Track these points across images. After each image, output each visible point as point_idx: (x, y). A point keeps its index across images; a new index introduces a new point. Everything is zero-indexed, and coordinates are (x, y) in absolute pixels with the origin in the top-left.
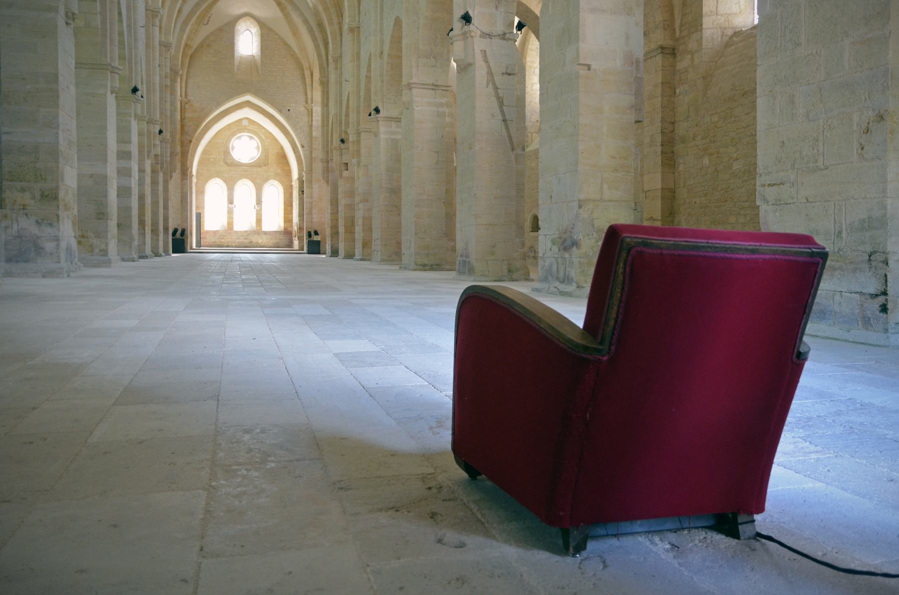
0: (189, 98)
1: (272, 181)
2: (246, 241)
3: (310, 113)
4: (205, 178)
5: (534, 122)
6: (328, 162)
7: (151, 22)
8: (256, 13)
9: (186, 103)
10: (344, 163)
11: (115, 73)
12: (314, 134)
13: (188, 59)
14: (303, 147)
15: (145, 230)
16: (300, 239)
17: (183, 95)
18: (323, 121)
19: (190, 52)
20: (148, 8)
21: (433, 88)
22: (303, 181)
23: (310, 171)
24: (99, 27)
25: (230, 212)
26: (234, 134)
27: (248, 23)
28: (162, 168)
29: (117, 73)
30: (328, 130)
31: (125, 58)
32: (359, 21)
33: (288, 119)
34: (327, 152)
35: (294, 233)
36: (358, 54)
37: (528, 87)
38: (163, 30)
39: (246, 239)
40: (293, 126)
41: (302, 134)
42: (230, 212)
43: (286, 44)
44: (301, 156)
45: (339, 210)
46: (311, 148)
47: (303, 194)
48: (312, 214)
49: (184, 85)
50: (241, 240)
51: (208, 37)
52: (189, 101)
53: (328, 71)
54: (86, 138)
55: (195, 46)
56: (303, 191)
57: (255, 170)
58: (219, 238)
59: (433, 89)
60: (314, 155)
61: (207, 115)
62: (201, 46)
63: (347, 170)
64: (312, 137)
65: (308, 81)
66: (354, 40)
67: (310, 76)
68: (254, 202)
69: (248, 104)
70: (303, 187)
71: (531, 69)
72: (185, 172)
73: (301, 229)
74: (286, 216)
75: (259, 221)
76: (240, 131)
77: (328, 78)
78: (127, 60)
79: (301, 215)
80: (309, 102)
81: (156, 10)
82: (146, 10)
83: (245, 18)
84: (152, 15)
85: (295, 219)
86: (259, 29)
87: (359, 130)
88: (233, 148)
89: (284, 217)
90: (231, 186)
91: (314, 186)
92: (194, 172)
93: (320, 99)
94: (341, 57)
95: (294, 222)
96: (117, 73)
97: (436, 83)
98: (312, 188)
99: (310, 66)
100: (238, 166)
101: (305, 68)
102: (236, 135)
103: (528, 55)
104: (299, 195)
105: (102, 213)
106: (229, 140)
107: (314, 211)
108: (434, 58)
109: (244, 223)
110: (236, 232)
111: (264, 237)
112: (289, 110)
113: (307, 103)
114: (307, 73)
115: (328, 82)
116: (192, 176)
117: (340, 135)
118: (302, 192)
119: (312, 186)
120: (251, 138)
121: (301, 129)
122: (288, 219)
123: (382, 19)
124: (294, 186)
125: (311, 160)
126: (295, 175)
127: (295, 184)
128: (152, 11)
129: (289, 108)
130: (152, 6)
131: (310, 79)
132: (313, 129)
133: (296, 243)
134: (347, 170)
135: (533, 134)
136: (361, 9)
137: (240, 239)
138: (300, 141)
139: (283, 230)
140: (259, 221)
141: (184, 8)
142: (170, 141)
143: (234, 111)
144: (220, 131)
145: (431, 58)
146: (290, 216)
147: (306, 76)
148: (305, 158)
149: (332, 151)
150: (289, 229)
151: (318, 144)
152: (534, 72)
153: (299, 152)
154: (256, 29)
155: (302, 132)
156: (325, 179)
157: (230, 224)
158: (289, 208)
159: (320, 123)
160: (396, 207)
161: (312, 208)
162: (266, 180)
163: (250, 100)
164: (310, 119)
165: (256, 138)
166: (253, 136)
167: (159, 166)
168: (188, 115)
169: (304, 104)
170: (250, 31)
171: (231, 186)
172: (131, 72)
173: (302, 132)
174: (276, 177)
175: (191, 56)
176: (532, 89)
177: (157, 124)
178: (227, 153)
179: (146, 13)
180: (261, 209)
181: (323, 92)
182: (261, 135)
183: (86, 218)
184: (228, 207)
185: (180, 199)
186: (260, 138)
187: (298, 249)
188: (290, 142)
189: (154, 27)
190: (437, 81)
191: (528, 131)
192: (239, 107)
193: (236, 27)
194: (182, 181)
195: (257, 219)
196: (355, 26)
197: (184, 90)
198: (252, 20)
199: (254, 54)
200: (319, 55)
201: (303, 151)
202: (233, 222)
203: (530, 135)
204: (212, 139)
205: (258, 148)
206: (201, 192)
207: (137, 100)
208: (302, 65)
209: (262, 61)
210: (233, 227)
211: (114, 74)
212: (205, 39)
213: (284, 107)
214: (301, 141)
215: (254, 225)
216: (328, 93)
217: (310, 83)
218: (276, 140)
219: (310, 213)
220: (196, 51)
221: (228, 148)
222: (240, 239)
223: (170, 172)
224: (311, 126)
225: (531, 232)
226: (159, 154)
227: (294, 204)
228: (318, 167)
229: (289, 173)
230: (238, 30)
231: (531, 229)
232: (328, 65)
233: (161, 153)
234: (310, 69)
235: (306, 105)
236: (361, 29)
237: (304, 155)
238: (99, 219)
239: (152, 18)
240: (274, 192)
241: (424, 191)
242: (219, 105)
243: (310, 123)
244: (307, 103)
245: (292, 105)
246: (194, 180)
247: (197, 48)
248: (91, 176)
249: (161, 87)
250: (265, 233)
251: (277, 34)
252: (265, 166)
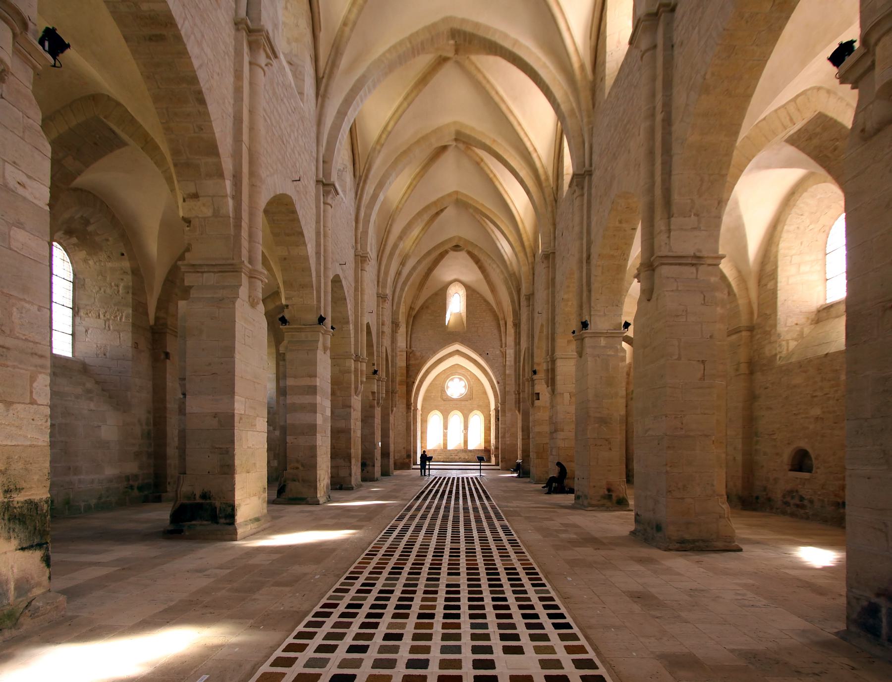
0: (413, 349)
1: (476, 412)
2: (457, 457)
3: (504, 355)
4: (426, 411)
5: (792, 326)
6: (520, 393)
7: (360, 267)
8: (464, 278)
9: (410, 353)
10: (536, 393)
11: (255, 278)
12: (507, 372)
13: (412, 319)
14: (498, 383)
15: (351, 463)
16: (497, 457)
17: (409, 347)
18: (515, 358)
19: (414, 313)
20: (357, 254)
21: (694, 262)
22: (499, 411)
23: (503, 403)
24: (231, 216)
25: (445, 435)
26: (448, 377)
27: (457, 287)
28: (378, 403)
29: (259, 279)
30: (519, 366)
31: (312, 287)
32: (555, 246)
33: (487, 361)
34: (519, 385)
35: (491, 451)
36: (553, 279)
37: (781, 282)
38: (380, 284)
39: (456, 456)
40: (491, 367)
41: (498, 372)
42: (445, 435)
43: (486, 301)
44: (497, 391)
45: (531, 437)
46: (505, 384)
47: (499, 421)
48: (505, 438)
49: (409, 339)
50: (453, 457)
51: (427, 301)
52: (413, 351)
53: (520, 314)
54: (210, 364)
55: (417, 309)
56: (498, 419)
57: (463, 403)
58: (438, 456)
59: (693, 265)
60: (507, 389)
61: (425, 362)
62: (422, 308)
63: (539, 399)
64: (505, 375)
65: (503, 329)
66: (549, 267)
67: (504, 325)
68: (462, 428)
69: (457, 352)
70: (499, 416)
71: (787, 258)
72: (409, 406)
73: (497, 448)
74: (486, 438)
75: (466, 442)
76: (452, 374)
77: (520, 319)
78: (314, 288)
79: (497, 437)
80: (503, 346)
81: (364, 255)
82: (355, 255)
83: (454, 283)
84: (361, 261)
85: (493, 441)
86: (465, 291)
87: (553, 357)
88: (448, 387)
89: (485, 439)
90: (446, 415)
91: (507, 415)
92: (419, 406)
93: (513, 344)
94: (533, 294)
95: (491, 443)
96: (259, 279)
97: (698, 254)
98: (505, 416)
99: (504, 316)
100: (451, 401)
101: (500, 319)
102: (449, 377)
103: (782, 239)
104: (496, 422)
105: (228, 466)
106: (445, 381)
107: (507, 435)
108: (697, 215)
109: (455, 443)
110: (449, 450)
111: (470, 454)
112: (488, 354)
113: (501, 347)
114: (502, 323)
115: (520, 324)
116: (416, 409)
117: (532, 366)
118: (497, 419)
119: (505, 415)
120: (461, 379)
121: (497, 369)
122: (487, 441)
123: (589, 217)
124: (492, 415)
125: (504, 393)
126: (493, 407)
127: (493, 413)
128: (361, 257)
129: (488, 352)
130: (360, 252)
131: (504, 327)
132: (507, 368)
133: (493, 459)
134: (539, 399)
135: (790, 341)
136: (556, 232)
137: (452, 455)
138: (496, 378)
139: (483, 449)
140: (466, 442)
141: (403, 271)
142: (386, 380)
143: (447, 358)
144: (436, 376)
145: (690, 216)
146: (489, 438)
147: (501, 325)
148: (500, 392)
149: (524, 384)
150: (488, 448)
151: (511, 381)
152: (791, 262)
153: (495, 388)
154: (463, 291)
155: (498, 371)
156: (521, 413)
157: (445, 445)
158: (488, 432)
159: (513, 363)
160: (607, 440)
161: (505, 433)
162: (471, 410)
163: (460, 349)
164: (504, 360)
165: (464, 379)
166: (462, 378)
167: (376, 401)
168: (412, 362)
169: (500, 348)
170: (459, 294)
171: (446, 415)
172: (319, 301)
173: (498, 371)
174: (479, 408)
175: (414, 317)
176: (788, 284)
177: (363, 362)
178: (443, 391)
179: (355, 259)
180: (467, 433)
181: (516, 332)
182: (468, 376)
183: (209, 472)
184: (444, 432)
185: (405, 427)
186: (467, 379)
187: (494, 464)
188: (494, 392)
189: (363, 271)
190: (700, 251)
191: (782, 338)
192: (450, 355)
193: (447, 291)
194: (407, 413)
195: (464, 441)
196: (550, 252)
197: (409, 343)
198: (460, 284)
199: (461, 312)
200: (513, 301)
201: (499, 387)
202: (447, 443)
203: (784, 343)
204: (432, 381)
205: (465, 386)
206: (424, 421)
207: (326, 331)
208: (498, 317)
209: (467, 316)
210: (447, 447)
211: (253, 280)
212: (424, 303)
213: (484, 351)
214: (497, 379)
215: (462, 445)
216: (520, 333)
217: (505, 331)
218: (479, 380)
219: (504, 437)
220: (418, 312)
221: (444, 388)
222: (452, 455)
223: (391, 407)
224: (505, 366)
225: (791, 470)
226: (376, 391)
227: (491, 429)
228: (511, 398)
229: (488, 405)
230: (450, 294)
231: (790, 467)
232: (520, 309)
233: (377, 390)
234: (504, 318)
235: (501, 349)
236: (557, 254)
237: (500, 390)
238: (225, 474)
239: (361, 263)
240: (477, 421)
241: (682, 424)
242: (435, 352)
243: (504, 363)
244: (501, 347)
245: (490, 350)
246: (419, 413)
247: (418, 310)
248: (215, 415)
249: (378, 334)
250: (471, 451)
251: (478, 293)
252: (471, 400)
